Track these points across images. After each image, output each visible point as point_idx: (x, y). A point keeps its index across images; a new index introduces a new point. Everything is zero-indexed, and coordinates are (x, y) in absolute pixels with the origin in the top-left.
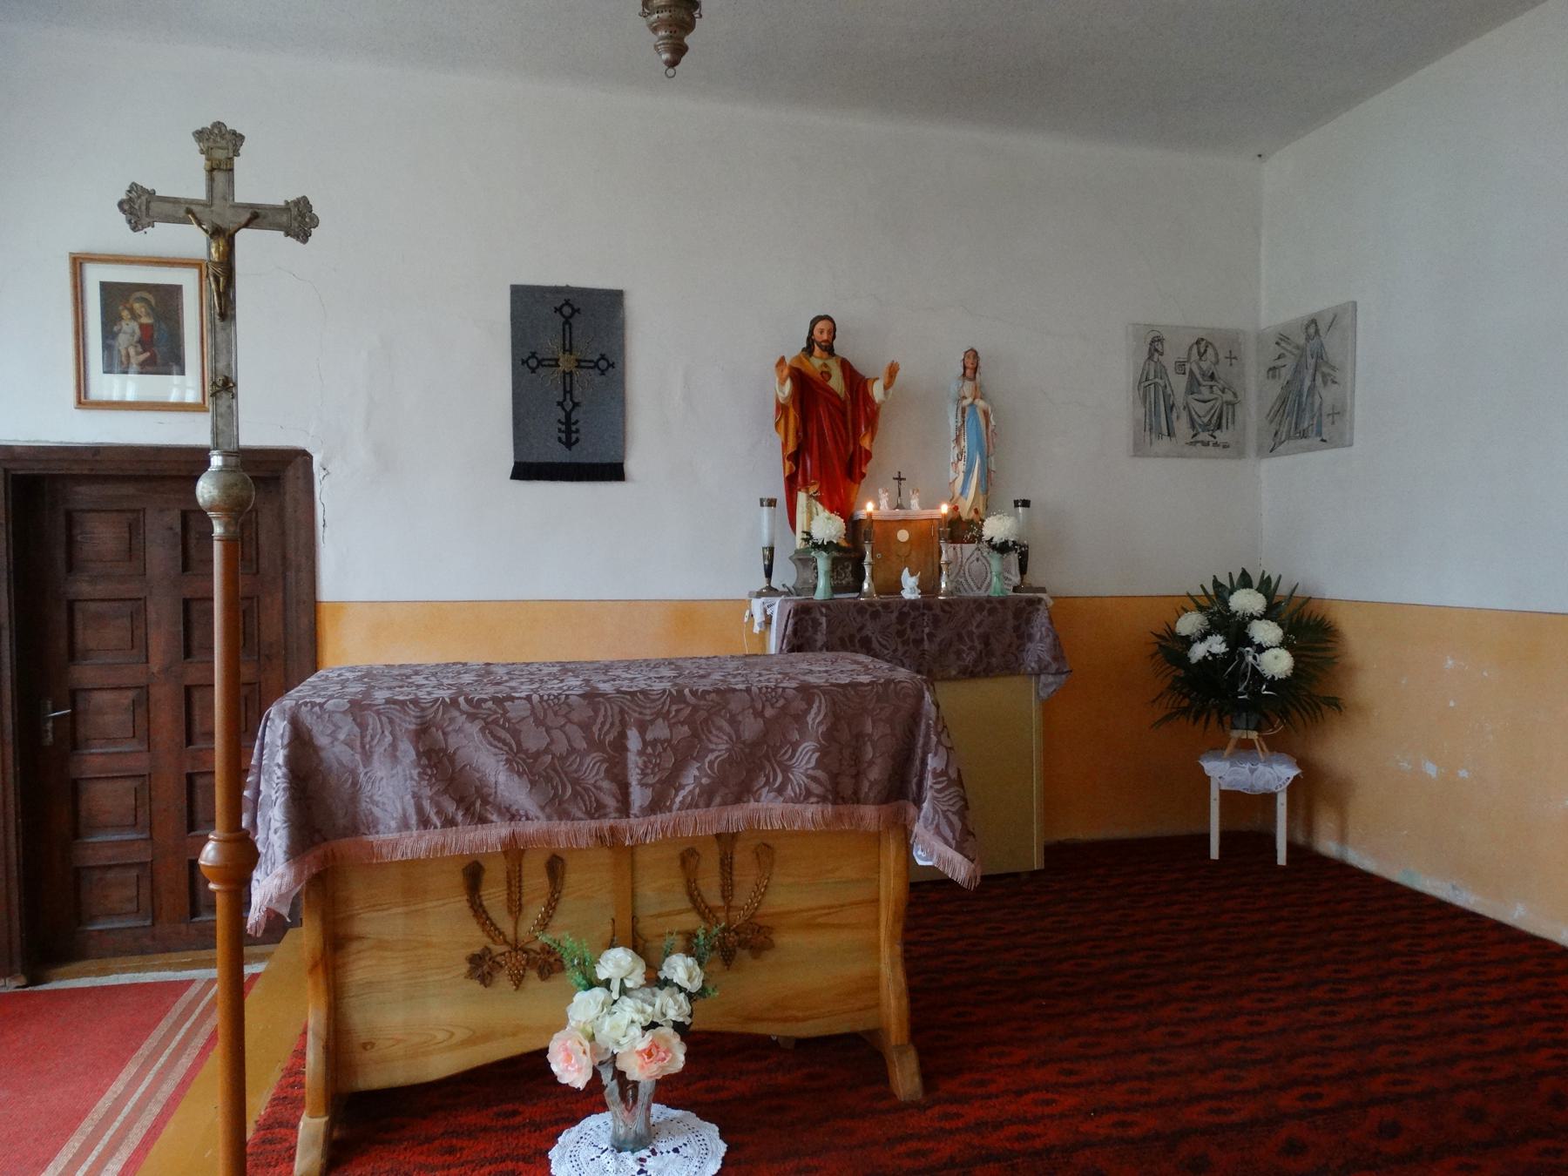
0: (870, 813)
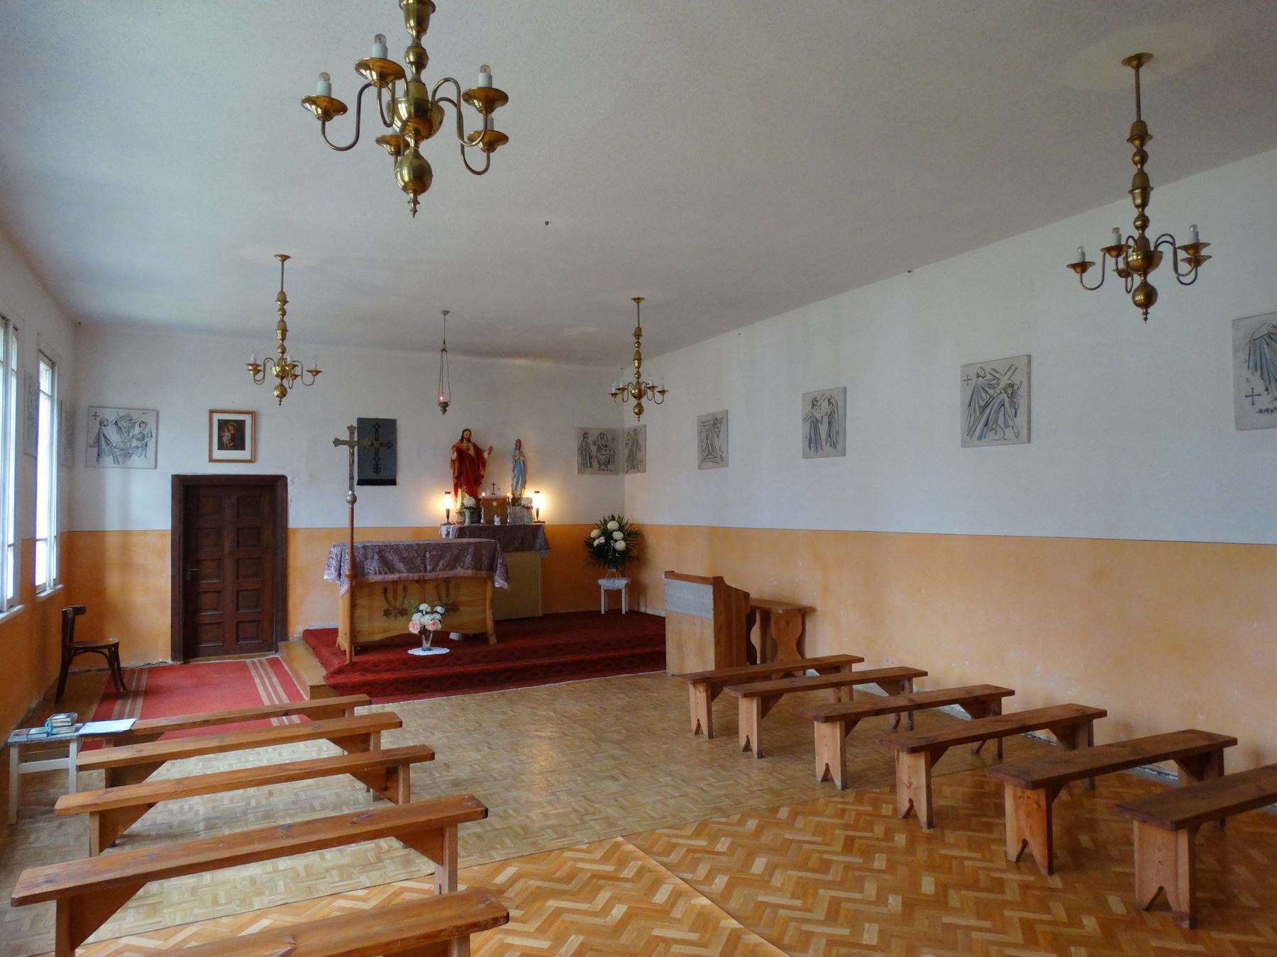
0: (484, 573)
